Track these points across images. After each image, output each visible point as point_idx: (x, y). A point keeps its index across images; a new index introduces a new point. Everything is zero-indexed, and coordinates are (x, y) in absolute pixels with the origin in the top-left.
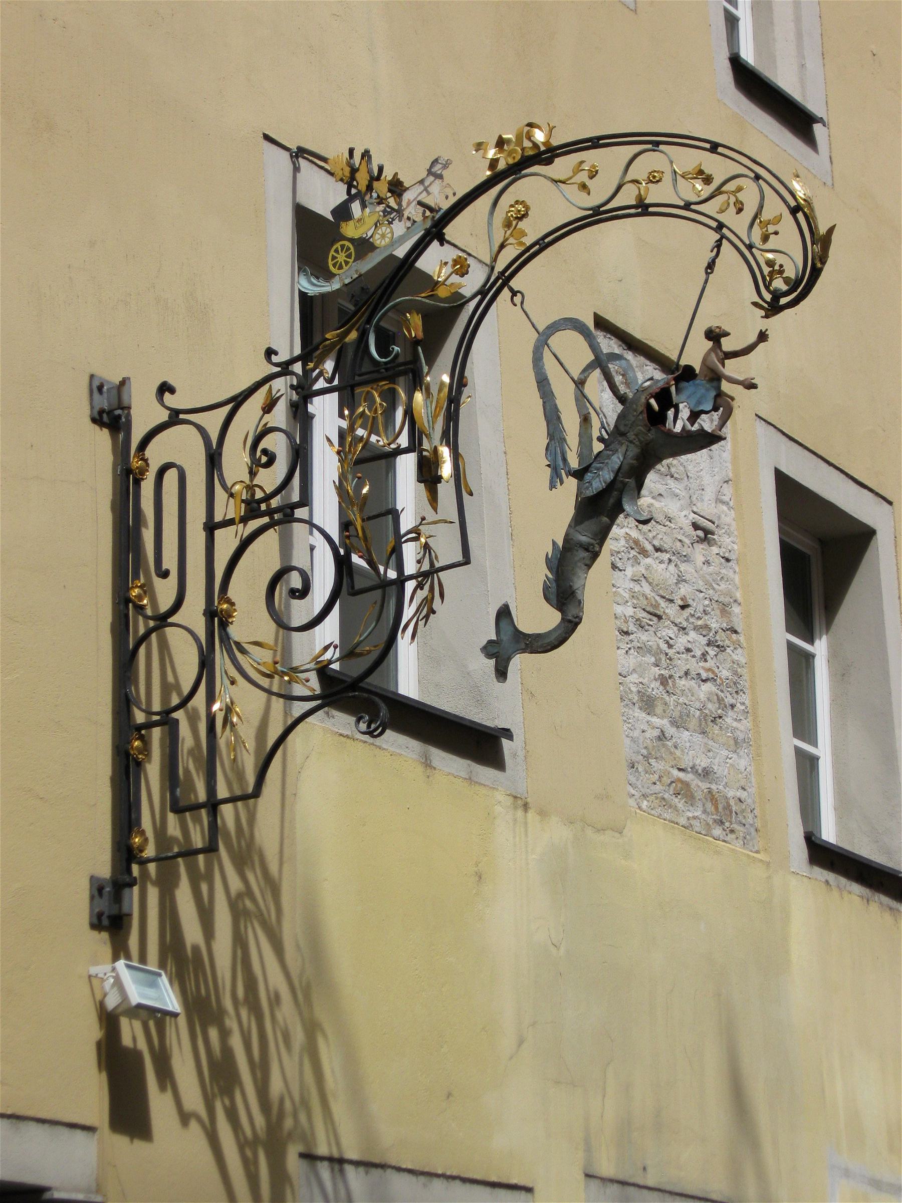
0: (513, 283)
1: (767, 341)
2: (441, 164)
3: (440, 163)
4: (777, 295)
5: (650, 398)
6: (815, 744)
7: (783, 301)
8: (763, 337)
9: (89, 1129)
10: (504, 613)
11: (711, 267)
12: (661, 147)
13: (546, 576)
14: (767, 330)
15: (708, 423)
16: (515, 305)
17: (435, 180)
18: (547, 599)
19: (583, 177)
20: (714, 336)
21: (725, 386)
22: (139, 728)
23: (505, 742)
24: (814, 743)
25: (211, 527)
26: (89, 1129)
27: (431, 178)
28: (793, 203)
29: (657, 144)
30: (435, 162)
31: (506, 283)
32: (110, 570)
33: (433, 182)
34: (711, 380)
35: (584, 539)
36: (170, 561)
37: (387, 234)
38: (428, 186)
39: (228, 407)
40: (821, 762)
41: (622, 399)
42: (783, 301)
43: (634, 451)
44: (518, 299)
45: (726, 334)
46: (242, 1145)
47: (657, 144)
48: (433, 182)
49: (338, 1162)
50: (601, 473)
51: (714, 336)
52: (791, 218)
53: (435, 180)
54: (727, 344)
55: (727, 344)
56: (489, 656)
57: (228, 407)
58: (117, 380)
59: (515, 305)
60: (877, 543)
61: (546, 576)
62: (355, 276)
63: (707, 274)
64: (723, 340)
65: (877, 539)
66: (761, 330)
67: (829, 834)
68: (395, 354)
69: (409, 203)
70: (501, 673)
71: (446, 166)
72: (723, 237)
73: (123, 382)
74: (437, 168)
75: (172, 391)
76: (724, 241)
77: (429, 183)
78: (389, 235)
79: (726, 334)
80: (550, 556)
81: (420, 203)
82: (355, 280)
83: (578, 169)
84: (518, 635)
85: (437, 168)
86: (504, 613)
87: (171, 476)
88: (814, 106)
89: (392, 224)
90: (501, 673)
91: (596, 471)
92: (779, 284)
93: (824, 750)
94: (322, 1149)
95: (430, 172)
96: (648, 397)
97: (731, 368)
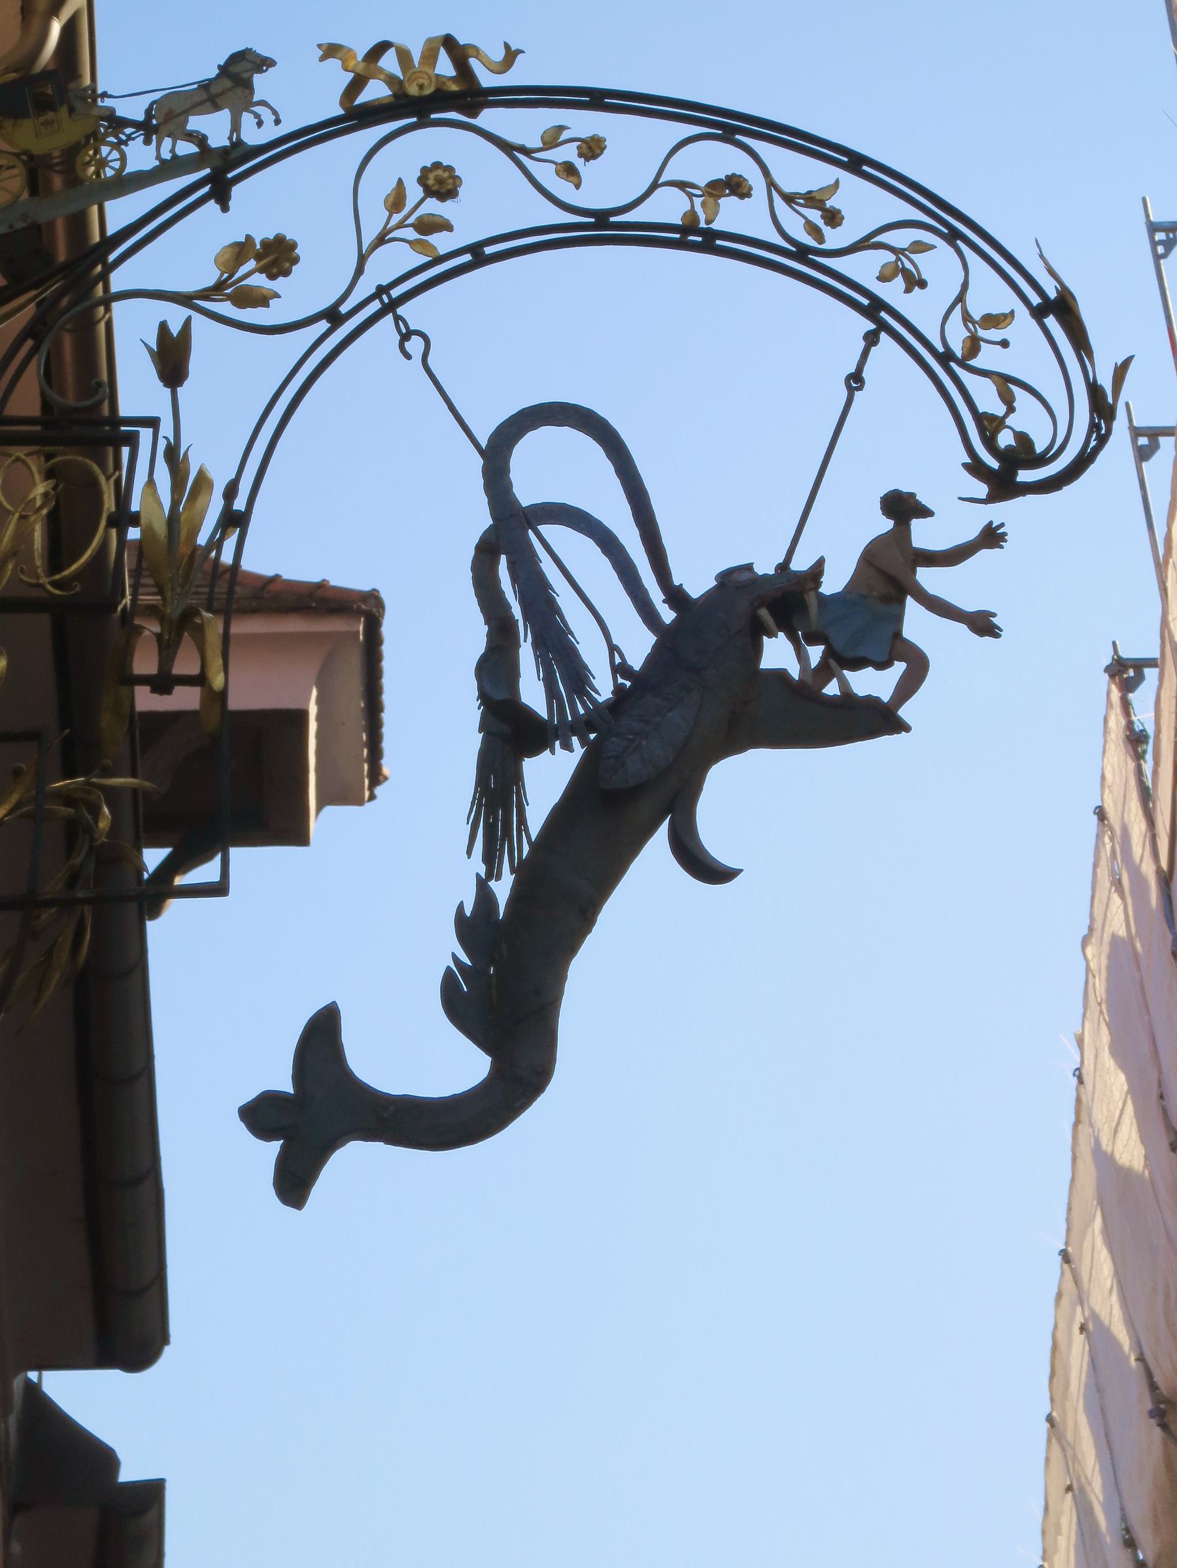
0: (400, 311)
1: (1002, 547)
2: (250, 62)
3: (248, 61)
5: (761, 605)
11: (855, 380)
13: (454, 956)
14: (1002, 525)
16: (408, 356)
17: (234, 87)
19: (568, 153)
27: (227, 83)
31: (391, 307)
32: (146, 1479)
33: (230, 89)
37: (111, 167)
38: (219, 95)
44: (415, 345)
45: (925, 512)
48: (230, 89)
50: (644, 743)
52: (1033, 323)
53: (234, 87)
55: (923, 534)
59: (408, 356)
61: (454, 956)
62: (20, 225)
63: (851, 392)
64: (916, 525)
66: (991, 523)
68: (710, 188)
72: (883, 326)
76: (883, 336)
77: (220, 90)
78: (117, 165)
79: (925, 512)
80: (468, 912)
82: (17, 231)
83: (552, 139)
89: (126, 145)
91: (631, 737)
96: (756, 604)
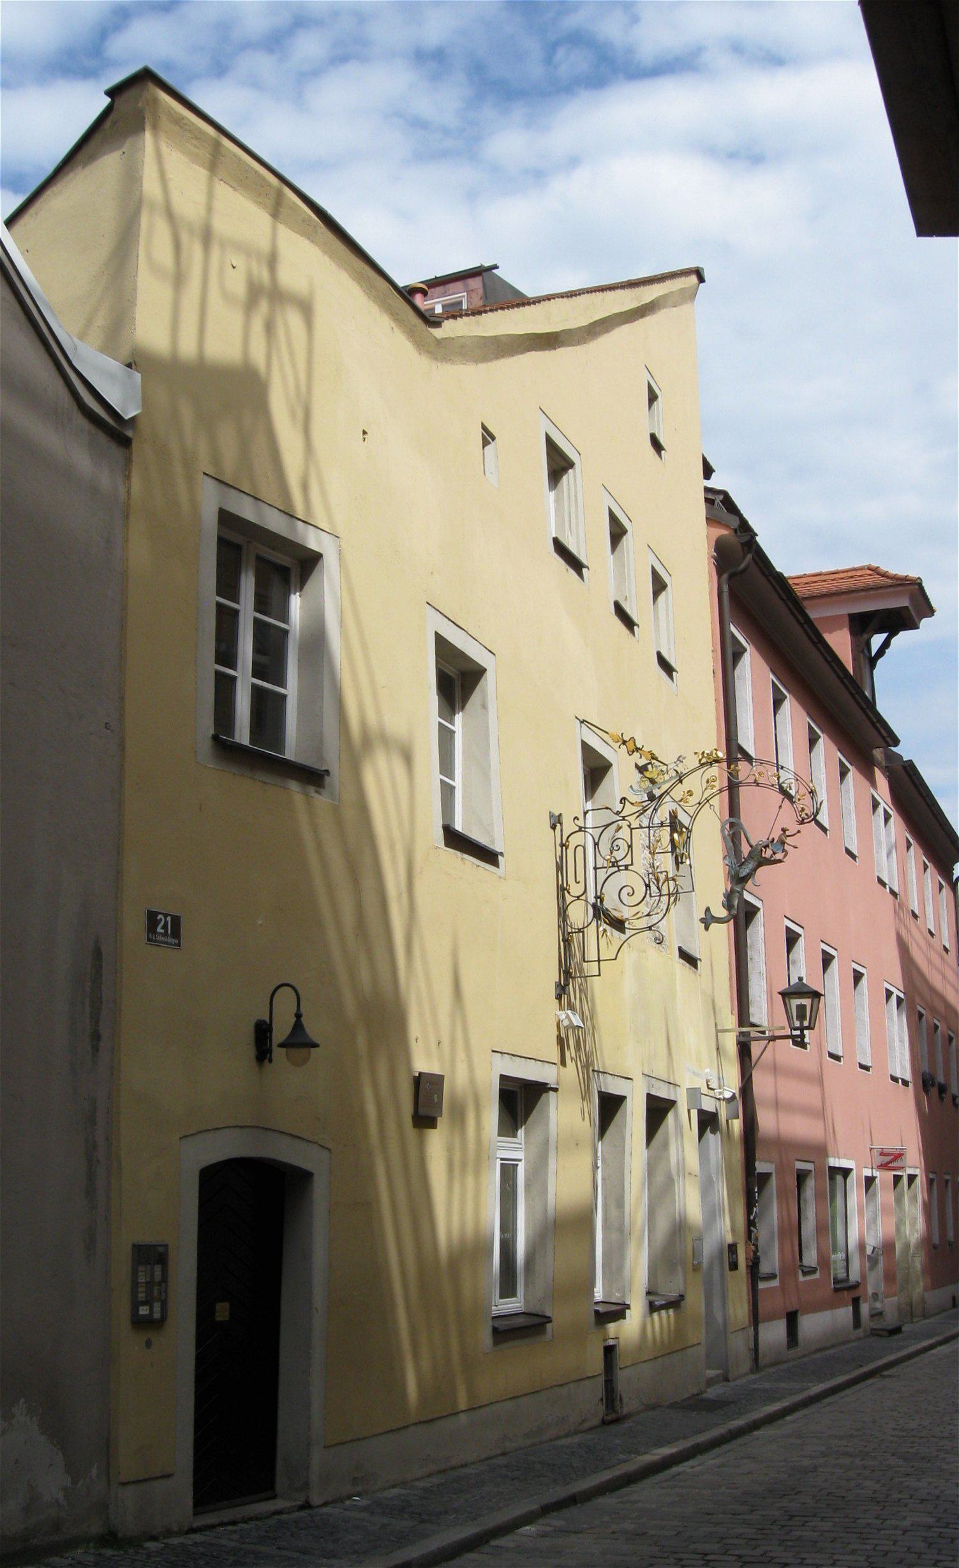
4: (803, 819)
6: (453, 779)
7: (805, 821)
8: (799, 832)
9: (554, 1064)
10: (708, 910)
12: (763, 765)
15: (779, 856)
18: (723, 906)
20: (784, 830)
21: (786, 847)
22: (569, 933)
23: (500, 857)
24: (452, 778)
25: (595, 868)
26: (554, 1064)
28: (810, 790)
29: (762, 763)
30: (680, 756)
34: (782, 844)
35: (739, 890)
36: (580, 878)
39: (604, 828)
40: (456, 791)
41: (751, 846)
42: (805, 821)
43: (756, 863)
44: (712, 807)
46: (582, 1067)
47: (762, 763)
49: (598, 1072)
51: (784, 830)
54: (788, 833)
55: (788, 833)
56: (702, 923)
57: (604, 828)
58: (557, 814)
60: (322, 572)
65: (486, 680)
67: (459, 826)
69: (671, 769)
70: (707, 928)
71: (684, 758)
73: (560, 815)
74: (681, 759)
75: (578, 819)
81: (675, 770)
84: (713, 917)
85: (681, 759)
86: (708, 910)
87: (580, 849)
88: (583, 559)
90: (707, 928)
92: (803, 815)
93: (458, 783)
94: (596, 1069)
95: (678, 760)
97: (788, 840)
